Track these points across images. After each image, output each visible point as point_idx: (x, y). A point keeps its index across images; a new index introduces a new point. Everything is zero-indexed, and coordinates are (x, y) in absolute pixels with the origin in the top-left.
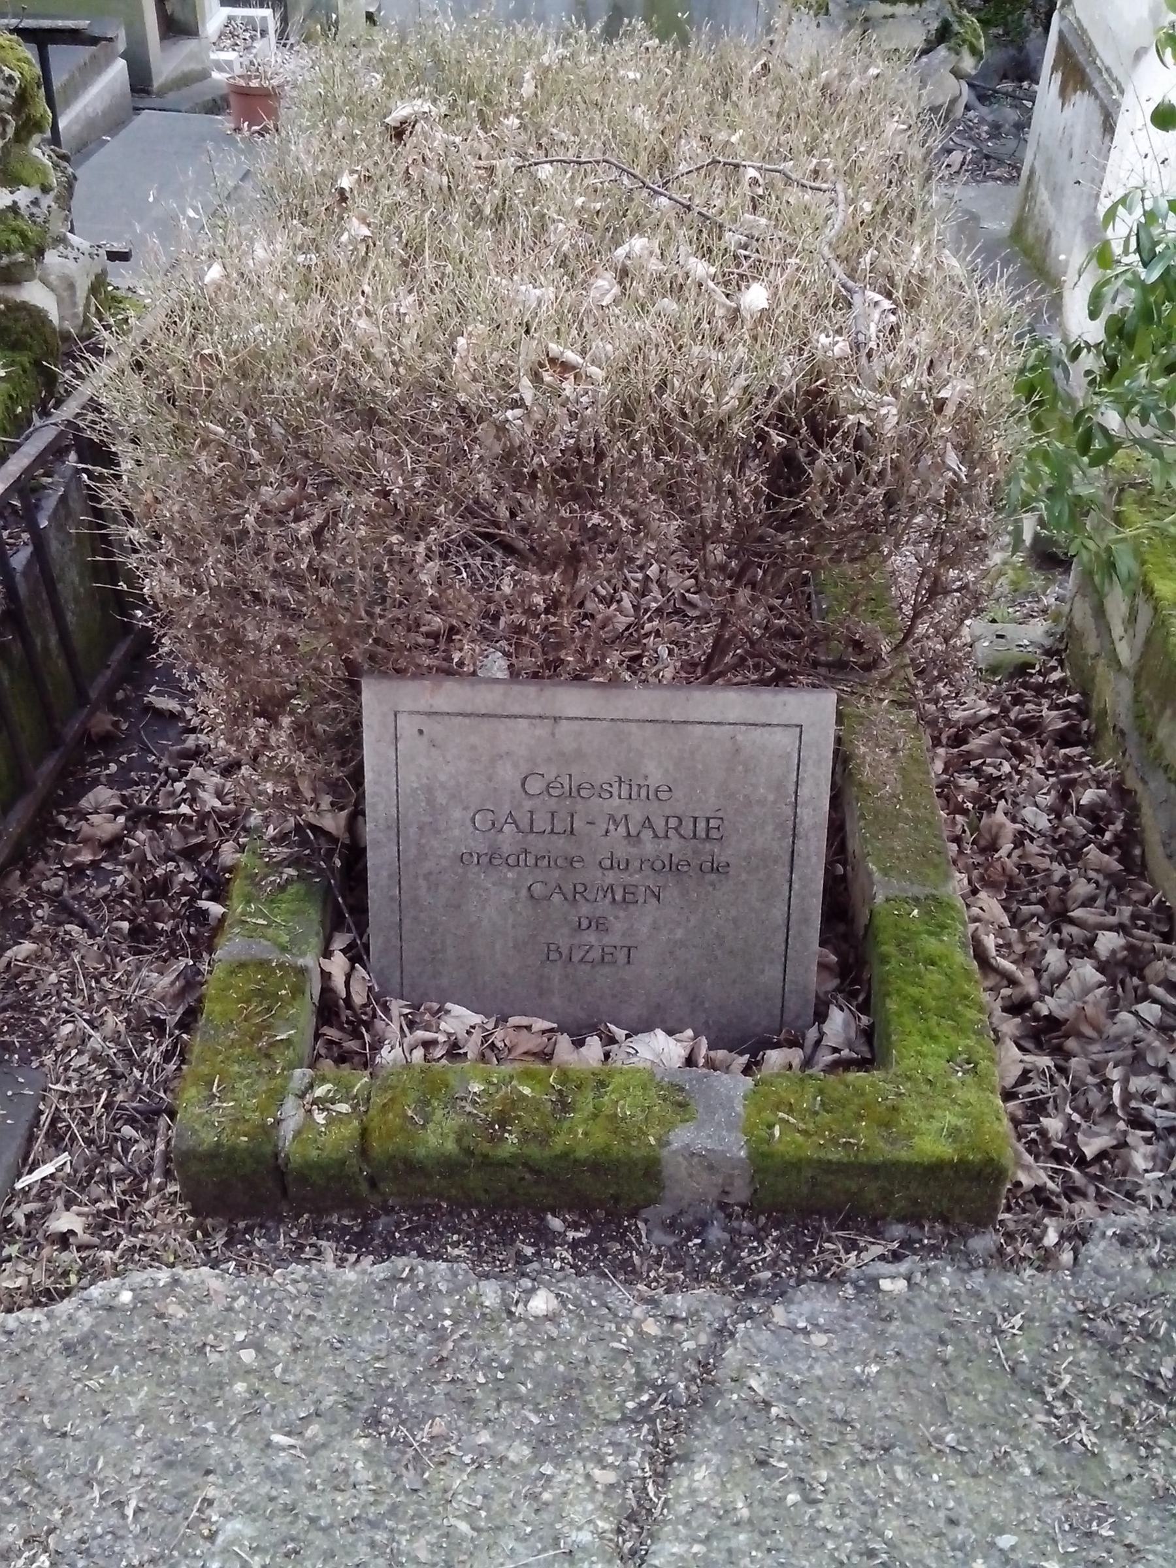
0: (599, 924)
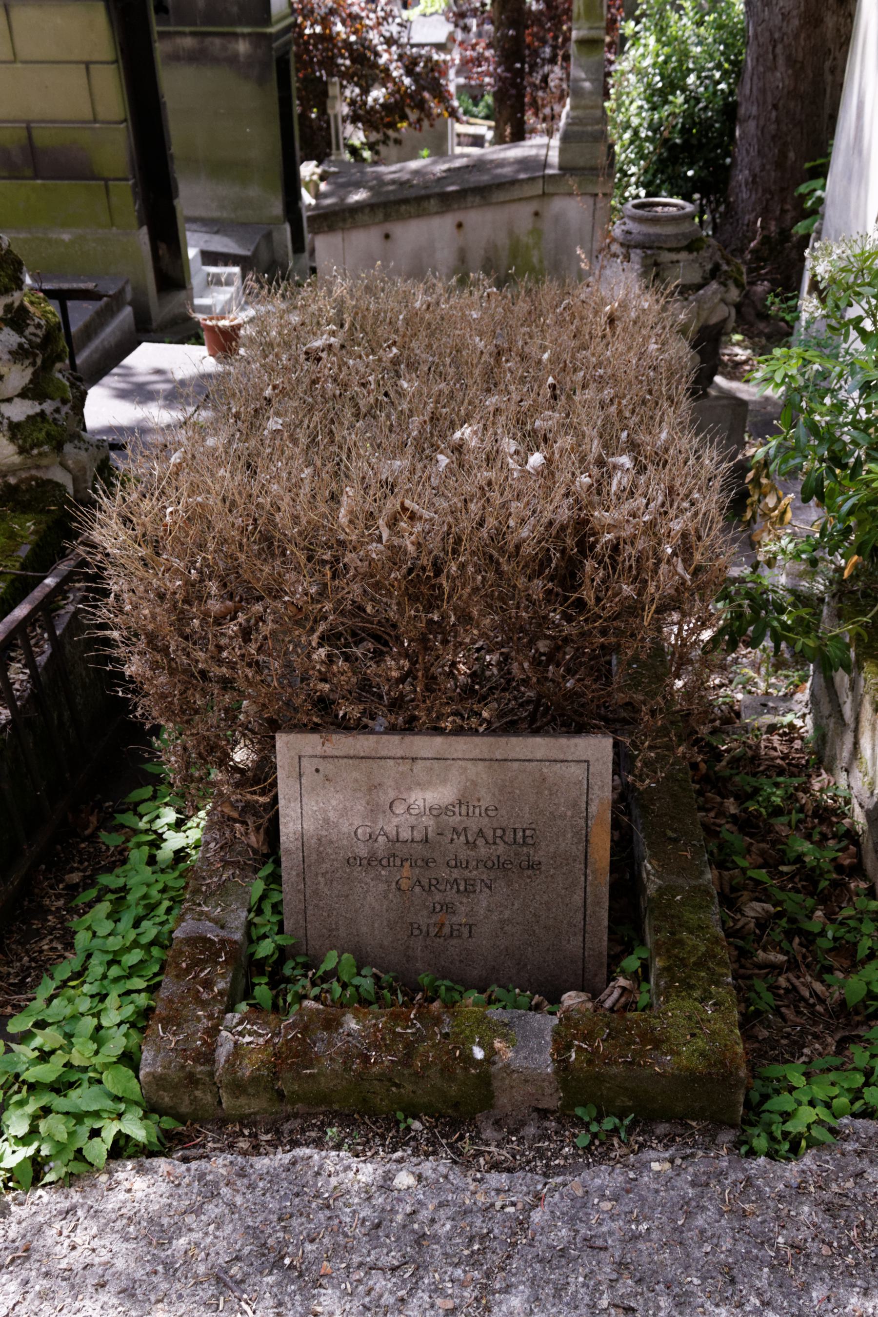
0: (448, 908)
